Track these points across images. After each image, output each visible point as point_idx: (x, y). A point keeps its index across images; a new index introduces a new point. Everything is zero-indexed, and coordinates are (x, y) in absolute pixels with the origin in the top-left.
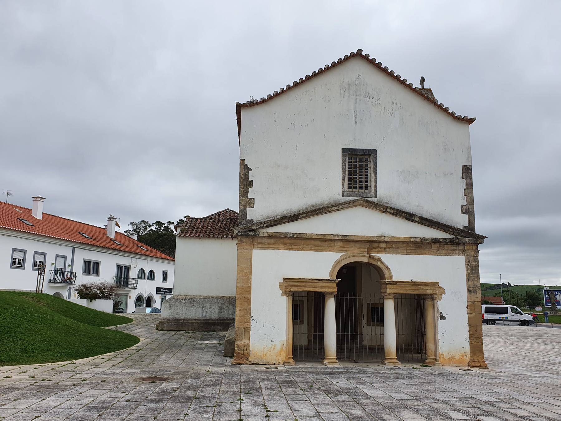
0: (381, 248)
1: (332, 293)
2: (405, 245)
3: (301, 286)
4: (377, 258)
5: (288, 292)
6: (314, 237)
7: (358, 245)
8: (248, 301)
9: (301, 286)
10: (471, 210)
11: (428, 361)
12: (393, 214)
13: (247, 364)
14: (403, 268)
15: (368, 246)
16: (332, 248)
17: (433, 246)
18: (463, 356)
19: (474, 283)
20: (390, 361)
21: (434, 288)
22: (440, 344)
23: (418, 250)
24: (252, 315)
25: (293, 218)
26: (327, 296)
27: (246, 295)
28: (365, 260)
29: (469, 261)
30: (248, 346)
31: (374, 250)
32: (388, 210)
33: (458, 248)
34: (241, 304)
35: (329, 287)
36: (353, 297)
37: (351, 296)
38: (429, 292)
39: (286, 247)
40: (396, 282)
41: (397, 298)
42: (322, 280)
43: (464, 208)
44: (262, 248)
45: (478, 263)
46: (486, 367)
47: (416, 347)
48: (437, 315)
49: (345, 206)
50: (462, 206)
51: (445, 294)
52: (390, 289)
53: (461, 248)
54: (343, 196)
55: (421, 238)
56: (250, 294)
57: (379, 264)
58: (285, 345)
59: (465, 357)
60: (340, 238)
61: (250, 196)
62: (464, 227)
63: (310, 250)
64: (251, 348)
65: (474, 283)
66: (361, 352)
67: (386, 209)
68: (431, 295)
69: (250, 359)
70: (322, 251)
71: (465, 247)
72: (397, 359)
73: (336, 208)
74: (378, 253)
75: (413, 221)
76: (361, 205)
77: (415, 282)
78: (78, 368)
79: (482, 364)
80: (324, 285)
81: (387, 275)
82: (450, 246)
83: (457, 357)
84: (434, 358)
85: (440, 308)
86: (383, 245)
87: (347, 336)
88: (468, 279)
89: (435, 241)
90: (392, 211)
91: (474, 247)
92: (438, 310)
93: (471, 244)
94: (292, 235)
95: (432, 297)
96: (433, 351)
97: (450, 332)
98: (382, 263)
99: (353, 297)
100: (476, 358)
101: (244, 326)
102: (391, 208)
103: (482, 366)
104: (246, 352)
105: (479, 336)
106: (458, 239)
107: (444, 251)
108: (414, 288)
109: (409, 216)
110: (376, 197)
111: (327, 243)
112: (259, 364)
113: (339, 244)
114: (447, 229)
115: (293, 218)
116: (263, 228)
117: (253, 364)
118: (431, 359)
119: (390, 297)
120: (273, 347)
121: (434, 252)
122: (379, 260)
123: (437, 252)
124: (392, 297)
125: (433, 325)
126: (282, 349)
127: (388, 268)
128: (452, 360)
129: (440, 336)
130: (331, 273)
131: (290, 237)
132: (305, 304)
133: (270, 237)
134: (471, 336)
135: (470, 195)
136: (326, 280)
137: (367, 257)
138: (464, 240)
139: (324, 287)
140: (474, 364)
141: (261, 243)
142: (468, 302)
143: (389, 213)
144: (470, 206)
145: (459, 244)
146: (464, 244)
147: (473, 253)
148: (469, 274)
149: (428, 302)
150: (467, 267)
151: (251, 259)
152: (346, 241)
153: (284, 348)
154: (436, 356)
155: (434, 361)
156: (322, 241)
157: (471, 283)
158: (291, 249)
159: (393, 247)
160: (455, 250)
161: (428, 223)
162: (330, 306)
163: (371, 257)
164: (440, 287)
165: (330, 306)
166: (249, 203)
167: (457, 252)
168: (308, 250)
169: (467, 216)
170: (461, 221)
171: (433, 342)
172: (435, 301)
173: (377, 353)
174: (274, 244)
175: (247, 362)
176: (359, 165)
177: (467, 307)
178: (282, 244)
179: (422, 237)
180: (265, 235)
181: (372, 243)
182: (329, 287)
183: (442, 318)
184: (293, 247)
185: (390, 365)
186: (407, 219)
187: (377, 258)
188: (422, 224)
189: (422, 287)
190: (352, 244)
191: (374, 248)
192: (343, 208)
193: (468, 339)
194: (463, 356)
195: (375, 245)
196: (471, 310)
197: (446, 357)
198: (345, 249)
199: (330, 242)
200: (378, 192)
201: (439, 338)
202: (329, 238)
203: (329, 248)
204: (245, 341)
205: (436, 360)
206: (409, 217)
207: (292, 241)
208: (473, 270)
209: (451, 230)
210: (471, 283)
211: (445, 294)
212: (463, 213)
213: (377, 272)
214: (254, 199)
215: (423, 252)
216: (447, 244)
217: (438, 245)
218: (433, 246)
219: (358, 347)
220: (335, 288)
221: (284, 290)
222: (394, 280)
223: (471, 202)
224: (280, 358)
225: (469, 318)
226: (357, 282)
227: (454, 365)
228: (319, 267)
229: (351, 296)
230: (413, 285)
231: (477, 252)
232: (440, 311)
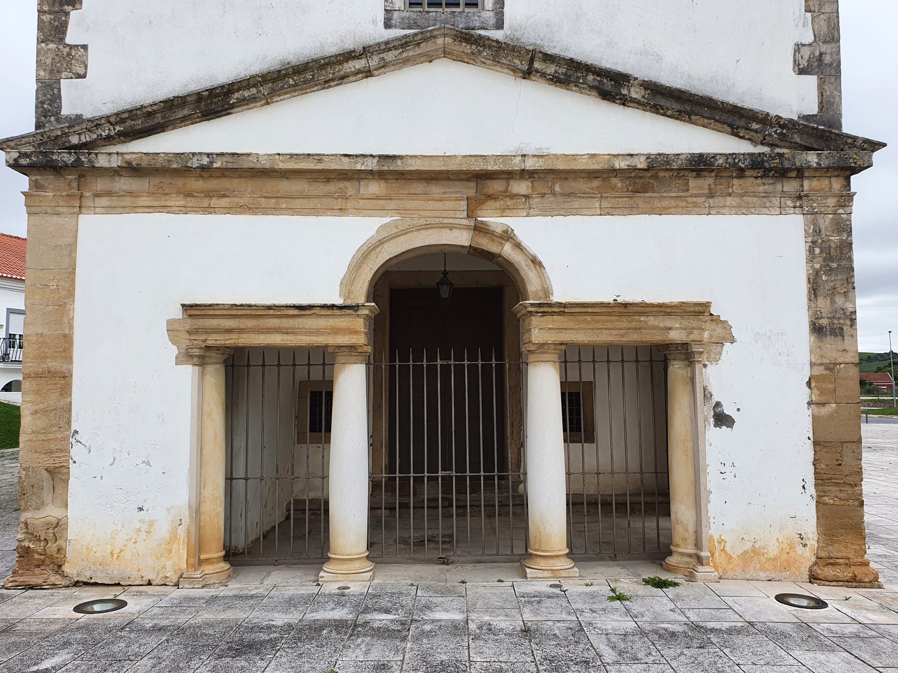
0: (513, 196)
1: (352, 348)
2: (596, 183)
3: (241, 331)
4: (499, 230)
5: (196, 352)
6: (282, 166)
7: (436, 190)
9: (241, 331)
10: (827, 59)
11: (672, 560)
12: (557, 81)
13: (54, 586)
14: (580, 260)
15: (471, 192)
16: (350, 204)
17: (692, 183)
18: (792, 546)
19: (833, 302)
20: (542, 564)
21: (694, 323)
22: (714, 508)
23: (640, 200)
24: (74, 426)
25: (214, 103)
26: (532, 358)
27: (54, 365)
28: (462, 238)
29: (817, 232)
30: (58, 526)
31: (491, 204)
32: (537, 65)
33: (779, 187)
34: (37, 392)
35: (336, 331)
36: (439, 362)
37: (432, 358)
38: (676, 336)
39: (191, 202)
40: (560, 305)
41: (569, 357)
42: (311, 307)
43: (806, 53)
44: (110, 210)
45: (850, 233)
46: (874, 582)
47: (634, 517)
48: (706, 412)
49: (390, 56)
50: (798, 47)
51: (733, 341)
52: (539, 331)
53: (790, 186)
54: (388, 25)
55: (648, 156)
56: (69, 359)
57: (507, 250)
58: (186, 521)
59: (800, 549)
60: (372, 165)
61: (71, 38)
63: (275, 210)
64: (71, 533)
65: (833, 302)
66: (490, 516)
67: (532, 61)
68: (685, 345)
69: (66, 568)
70: (315, 212)
71: (806, 184)
72: (567, 555)
73: (359, 64)
74: (504, 211)
75: (625, 101)
76: (446, 54)
77: (625, 305)
79: (858, 571)
80: (322, 323)
81: (533, 284)
82: (749, 183)
83: (773, 550)
84: (691, 550)
85: (713, 389)
86: (521, 187)
87: (475, 467)
88: (814, 290)
89: (700, 165)
90: (551, 69)
91: (837, 184)
92: (707, 396)
93: (822, 171)
94: (205, 161)
95: (686, 353)
96: (691, 529)
97: (748, 471)
98: (518, 246)
99: (439, 362)
100: (836, 551)
101: (49, 462)
102: (549, 58)
103: (861, 579)
104: (52, 548)
105: (850, 480)
106: (781, 155)
107: (729, 200)
108: (625, 324)
109: (608, 85)
110: (499, 25)
111: (332, 187)
112: (96, 584)
113: (374, 188)
114: (742, 123)
115: (214, 103)
116: (109, 140)
117: (77, 584)
118: (682, 554)
119: (545, 357)
120: (145, 527)
121: (696, 205)
122: (507, 236)
123: (709, 203)
124: (554, 357)
125: (690, 445)
126: (174, 537)
127: (535, 262)
128: (751, 562)
129: (712, 480)
130: (347, 284)
131: (203, 168)
132: (260, 378)
133: (133, 169)
134: (821, 479)
135: (827, 8)
136: (324, 307)
137: (467, 228)
138: (800, 156)
139: (318, 332)
140: (829, 572)
141: (109, 194)
142: (812, 365)
143: (543, 75)
144: (824, 48)
145: (782, 174)
146: (800, 173)
147: (831, 202)
148: (817, 273)
149: (677, 369)
150: (811, 251)
151: (72, 247)
152: (393, 175)
153: (182, 532)
154: (698, 545)
155: (693, 561)
156: (315, 180)
158: (209, 210)
159: (554, 194)
160: (767, 195)
161: (677, 106)
162: (351, 391)
163: (480, 229)
164: (715, 319)
165: (351, 391)
166: (69, 63)
167: (776, 201)
168: (266, 211)
170: (796, 98)
171: (690, 500)
172: (698, 367)
174: (151, 194)
175: (55, 579)
177: (809, 384)
178: (179, 193)
179: (654, 151)
180: (115, 162)
181: (482, 181)
182: (336, 331)
183: (722, 420)
184: (214, 202)
185: (537, 582)
186: (606, 96)
187: (499, 230)
188: (657, 109)
189: (652, 321)
190: (419, 187)
191: (490, 197)
192: (384, 66)
193: (811, 490)
194: (792, 546)
195: (496, 186)
196: (822, 393)
197: (735, 548)
198: (392, 204)
199: (341, 184)
200: (506, 10)
201: (710, 486)
202: (334, 166)
203: (339, 204)
204: (51, 512)
205: (700, 560)
206: (611, 86)
207: (213, 184)
208: (832, 259)
209: (755, 126)
211: (733, 341)
212: (802, 71)
214: (85, 47)
215: (657, 204)
216: (741, 173)
217: (710, 181)
218: (692, 183)
220: (356, 332)
221: (185, 343)
222: (556, 298)
223: (830, 35)
224: (169, 564)
225: (816, 420)
227: (762, 575)
228: (309, 264)
229: (432, 358)
230: (621, 315)
231: (846, 198)
232: (716, 398)
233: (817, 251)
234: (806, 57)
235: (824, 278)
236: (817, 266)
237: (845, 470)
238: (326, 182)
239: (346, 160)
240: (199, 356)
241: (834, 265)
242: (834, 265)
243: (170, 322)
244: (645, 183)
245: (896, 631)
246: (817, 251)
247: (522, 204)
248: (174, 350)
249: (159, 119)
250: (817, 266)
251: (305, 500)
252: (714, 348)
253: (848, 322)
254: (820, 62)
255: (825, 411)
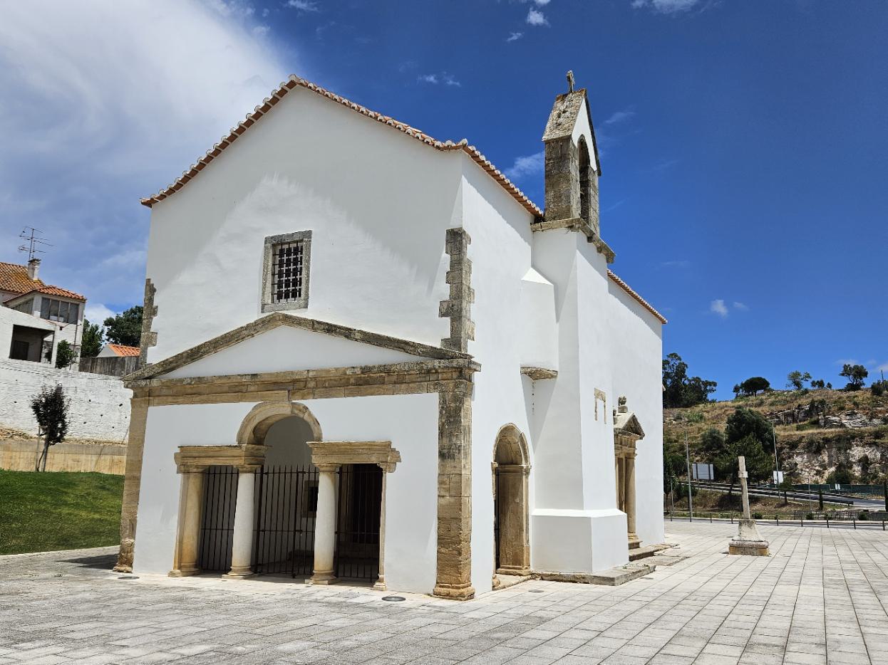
8: (137, 480)
14: (342, 422)
29: (444, 402)
34: (129, 486)
43: (445, 306)
44: (159, 404)
47: (359, 558)
51: (400, 461)
56: (140, 471)
57: (306, 417)
62: (445, 341)
78: (206, 623)
88: (441, 434)
98: (310, 414)
115: (194, 355)
132: (212, 483)
148: (443, 424)
150: (441, 412)
157: (445, 441)
162: (245, 486)
164: (394, 450)
165: (245, 486)
169: (448, 320)
173: (132, 544)
176: (288, 264)
181: (295, 385)
186: (193, 360)
210: (445, 441)
212: (442, 315)
213: (301, 428)
219: (282, 558)
226: (278, 449)
228: (221, 425)
233: (444, 412)
234: (445, 307)
235: (447, 427)
236: (444, 421)
237: (452, 533)
238: (234, 388)
239: (239, 377)
240: (184, 469)
241: (452, 420)
242: (452, 420)
243: (176, 454)
244: (364, 382)
245: (1, 571)
246: (444, 412)
247: (313, 394)
248: (176, 467)
249: (174, 365)
250: (444, 421)
251: (749, 496)
252: (392, 465)
253: (457, 451)
254: (453, 310)
255: (443, 501)
